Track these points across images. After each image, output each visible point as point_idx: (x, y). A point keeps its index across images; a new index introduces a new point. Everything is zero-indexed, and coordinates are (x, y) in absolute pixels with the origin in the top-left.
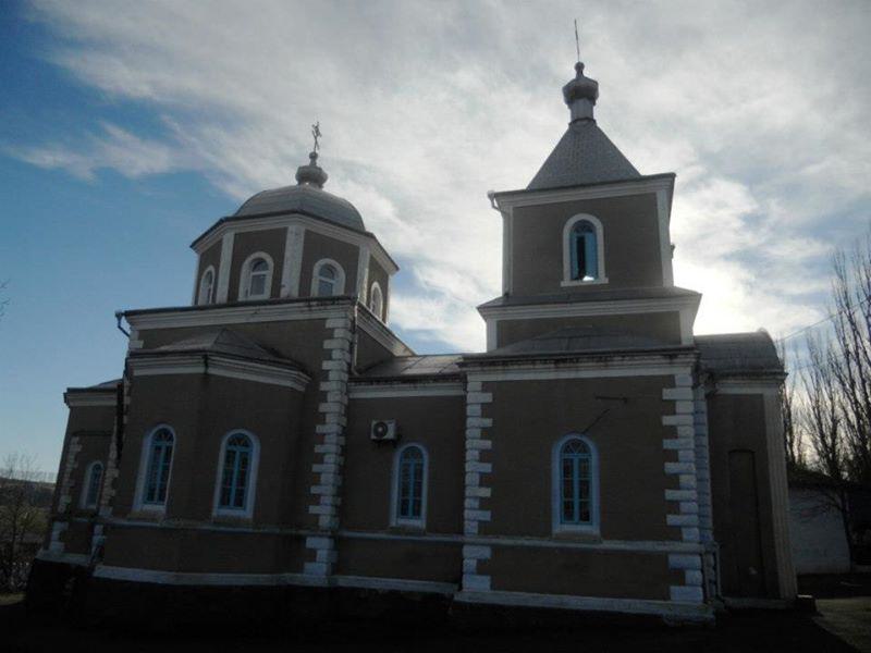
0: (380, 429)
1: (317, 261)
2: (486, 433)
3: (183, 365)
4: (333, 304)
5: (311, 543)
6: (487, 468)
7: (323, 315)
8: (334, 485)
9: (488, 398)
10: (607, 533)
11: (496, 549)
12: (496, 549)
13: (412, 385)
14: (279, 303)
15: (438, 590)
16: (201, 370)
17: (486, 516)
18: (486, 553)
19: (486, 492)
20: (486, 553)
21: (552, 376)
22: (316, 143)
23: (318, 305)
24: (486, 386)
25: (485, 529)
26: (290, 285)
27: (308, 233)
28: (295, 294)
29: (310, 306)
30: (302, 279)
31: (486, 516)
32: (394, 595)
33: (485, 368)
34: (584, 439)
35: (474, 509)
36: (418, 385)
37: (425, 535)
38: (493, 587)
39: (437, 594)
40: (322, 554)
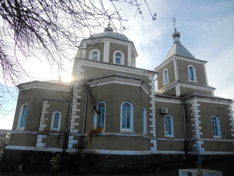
0: (164, 110)
1: (114, 51)
2: (199, 114)
3: (134, 83)
4: (152, 73)
5: (152, 141)
6: (200, 122)
7: (148, 75)
8: (195, 123)
9: (199, 105)
10: (223, 138)
11: (204, 141)
12: (204, 141)
13: (169, 99)
14: (87, 60)
15: (180, 153)
16: (140, 85)
17: (201, 134)
18: (202, 143)
19: (201, 128)
20: (202, 143)
21: (210, 102)
22: (86, 6)
23: (147, 72)
24: (198, 102)
25: (202, 137)
26: (106, 59)
27: (111, 43)
28: (108, 62)
29: (145, 72)
30: (127, 59)
31: (201, 134)
32: (170, 155)
33: (199, 98)
34: (216, 117)
35: (72, 140)
36: (170, 99)
37: (174, 139)
38: (205, 151)
39: (180, 154)
40: (155, 145)
